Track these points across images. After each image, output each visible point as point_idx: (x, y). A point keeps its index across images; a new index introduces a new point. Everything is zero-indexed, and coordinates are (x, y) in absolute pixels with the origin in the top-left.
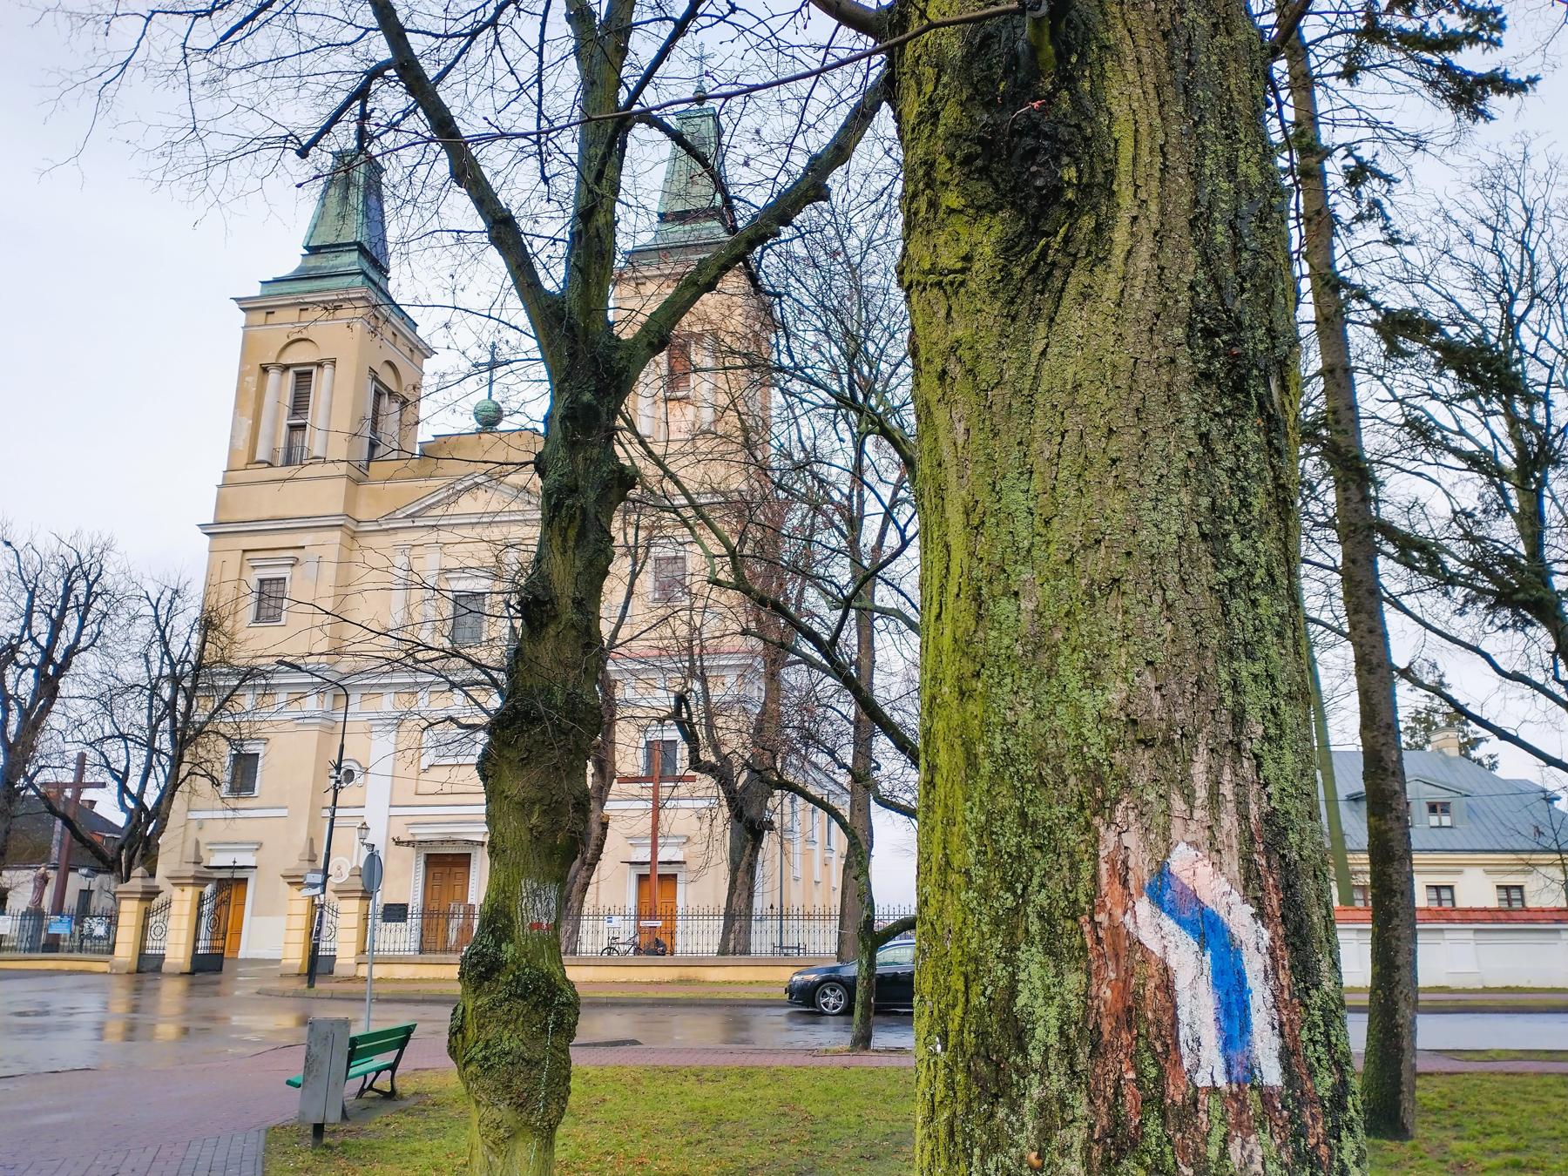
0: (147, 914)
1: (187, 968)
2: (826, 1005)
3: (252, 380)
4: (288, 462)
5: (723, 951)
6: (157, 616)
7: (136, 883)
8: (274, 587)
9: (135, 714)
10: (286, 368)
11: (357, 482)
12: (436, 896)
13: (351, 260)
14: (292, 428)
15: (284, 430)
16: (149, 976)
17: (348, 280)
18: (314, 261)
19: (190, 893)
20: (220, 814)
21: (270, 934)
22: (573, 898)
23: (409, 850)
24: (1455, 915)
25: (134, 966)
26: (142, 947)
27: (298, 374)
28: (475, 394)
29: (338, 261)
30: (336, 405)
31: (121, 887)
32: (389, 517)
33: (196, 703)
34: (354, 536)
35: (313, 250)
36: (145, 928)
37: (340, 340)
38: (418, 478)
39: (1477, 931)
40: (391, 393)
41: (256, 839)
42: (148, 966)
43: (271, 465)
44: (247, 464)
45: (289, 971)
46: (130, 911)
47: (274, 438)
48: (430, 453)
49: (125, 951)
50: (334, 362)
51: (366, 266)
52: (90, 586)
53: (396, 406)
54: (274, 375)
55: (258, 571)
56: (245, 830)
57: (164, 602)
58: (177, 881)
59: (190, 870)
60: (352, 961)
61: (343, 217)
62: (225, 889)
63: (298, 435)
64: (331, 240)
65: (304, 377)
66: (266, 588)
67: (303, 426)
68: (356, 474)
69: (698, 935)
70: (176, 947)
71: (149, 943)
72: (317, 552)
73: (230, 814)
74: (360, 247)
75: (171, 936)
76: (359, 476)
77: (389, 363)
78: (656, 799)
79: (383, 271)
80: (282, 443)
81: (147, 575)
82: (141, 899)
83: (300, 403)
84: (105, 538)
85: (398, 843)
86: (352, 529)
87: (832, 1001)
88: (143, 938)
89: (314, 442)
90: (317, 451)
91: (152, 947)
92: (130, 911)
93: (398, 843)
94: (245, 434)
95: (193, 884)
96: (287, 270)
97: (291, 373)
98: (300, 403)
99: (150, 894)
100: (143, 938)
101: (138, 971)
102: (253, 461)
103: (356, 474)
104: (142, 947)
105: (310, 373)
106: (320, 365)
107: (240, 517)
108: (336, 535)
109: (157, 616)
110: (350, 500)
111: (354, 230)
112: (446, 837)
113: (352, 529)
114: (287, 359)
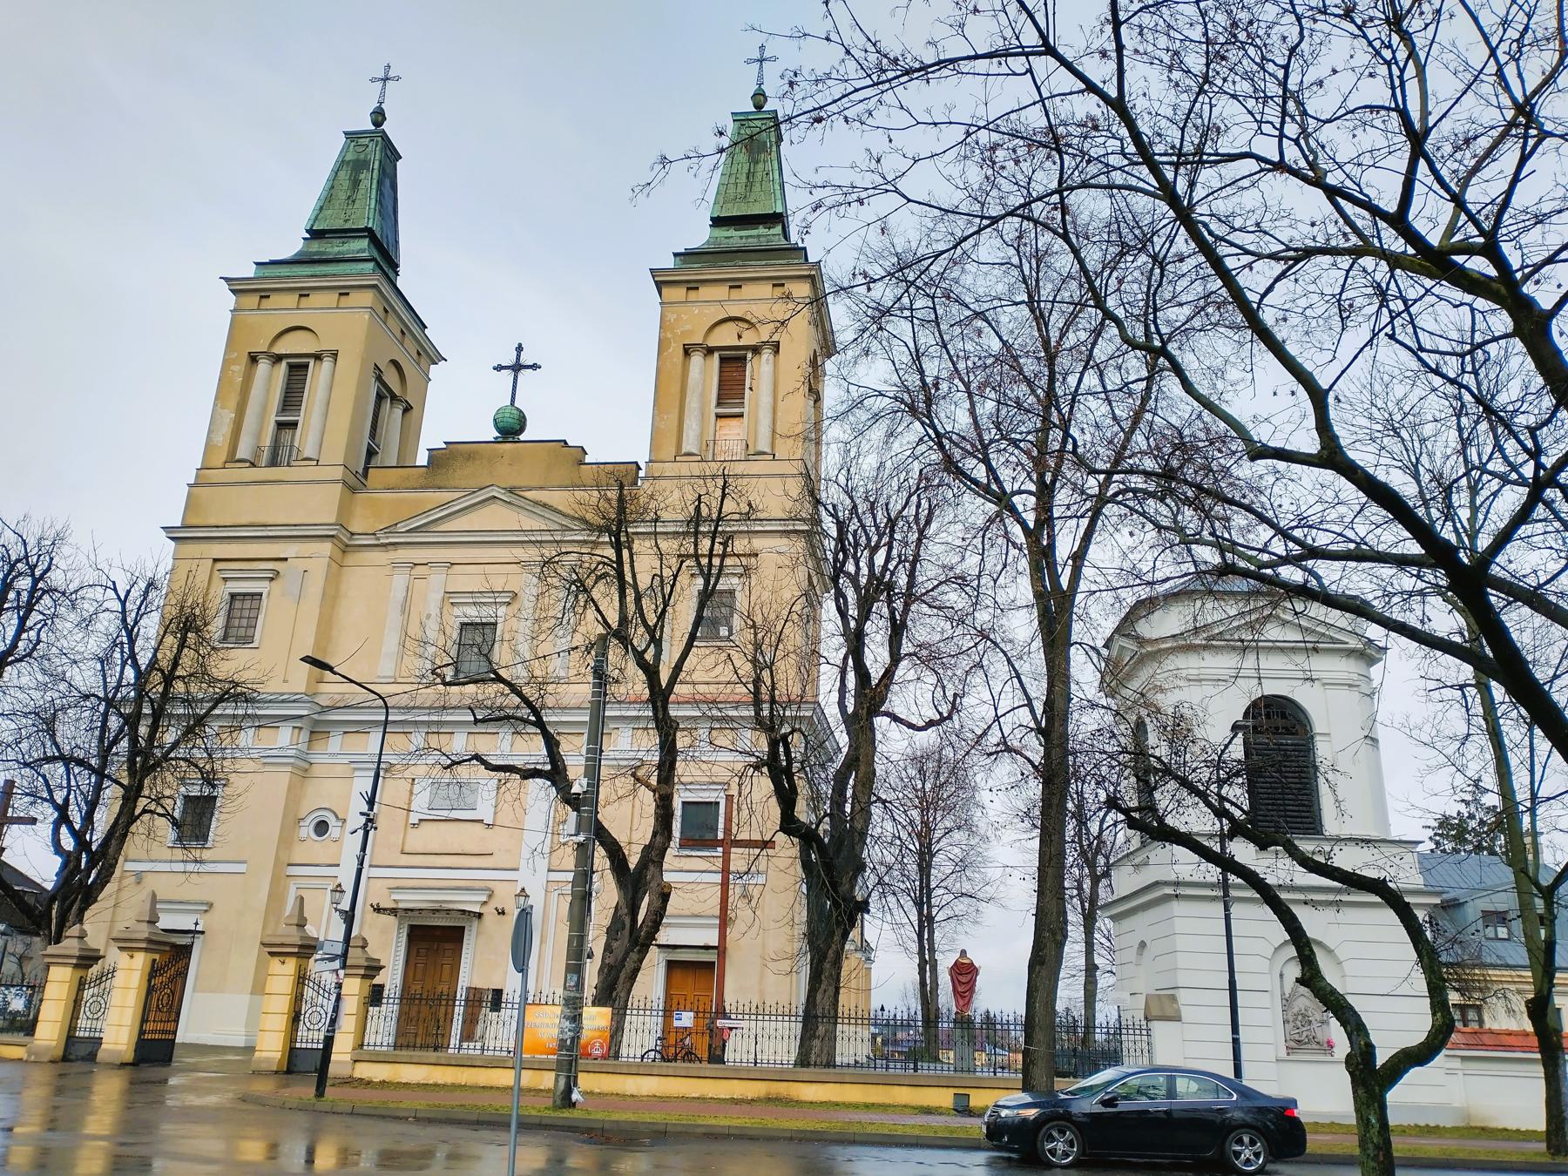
0: (82, 985)
1: (129, 1056)
2: (1053, 1152)
3: (239, 369)
4: (274, 462)
5: (803, 1061)
6: (124, 612)
7: (70, 945)
8: (247, 604)
9: (76, 733)
10: (278, 358)
11: (353, 490)
12: (419, 976)
13: (361, 246)
14: (281, 425)
15: (271, 427)
16: (77, 1067)
17: (361, 266)
18: (316, 246)
19: (141, 961)
20: (180, 867)
21: (230, 1012)
22: (619, 986)
23: (391, 920)
24: (1486, 1039)
25: (60, 1053)
26: (72, 1028)
27: (291, 367)
28: (497, 392)
29: (346, 247)
30: (332, 411)
31: (51, 949)
32: (390, 529)
33: (158, 730)
34: (346, 549)
35: (315, 234)
36: (77, 1003)
37: (342, 325)
38: (424, 487)
39: (1464, 1058)
40: (394, 397)
41: (210, 899)
42: (79, 1052)
43: (253, 465)
44: (224, 462)
45: (264, 1066)
46: (60, 982)
47: (259, 435)
48: (443, 458)
49: (49, 1032)
50: (335, 355)
51: (376, 254)
52: (36, 581)
53: (398, 411)
54: (263, 366)
55: (229, 584)
56: (196, 890)
57: (135, 593)
58: (127, 944)
59: (144, 931)
60: (348, 1058)
61: (351, 200)
62: (171, 959)
63: (286, 435)
64: (338, 224)
65: (298, 370)
66: (238, 604)
67: (294, 425)
68: (352, 480)
69: (764, 1038)
70: (118, 1030)
71: (82, 1022)
72: (303, 564)
73: (191, 867)
74: (369, 233)
75: (113, 1016)
76: (357, 480)
77: (395, 363)
78: (725, 871)
79: (394, 266)
80: (267, 441)
81: (116, 563)
82: (76, 966)
83: (292, 397)
84: (59, 527)
85: (378, 910)
86: (345, 543)
87: (1061, 1147)
88: (75, 1016)
89: (306, 439)
90: (307, 453)
91: (84, 1025)
92: (60, 982)
93: (378, 910)
94: (225, 430)
95: (146, 950)
96: (288, 253)
97: (283, 367)
98: (292, 397)
99: (88, 959)
100: (75, 1016)
101: (65, 1058)
102: (232, 459)
103: (352, 480)
104: (72, 1028)
105: (306, 366)
106: (318, 357)
107: (213, 522)
108: (326, 548)
109: (124, 612)
110: (344, 509)
111: (365, 215)
112: (436, 906)
113: (345, 543)
114: (280, 349)
